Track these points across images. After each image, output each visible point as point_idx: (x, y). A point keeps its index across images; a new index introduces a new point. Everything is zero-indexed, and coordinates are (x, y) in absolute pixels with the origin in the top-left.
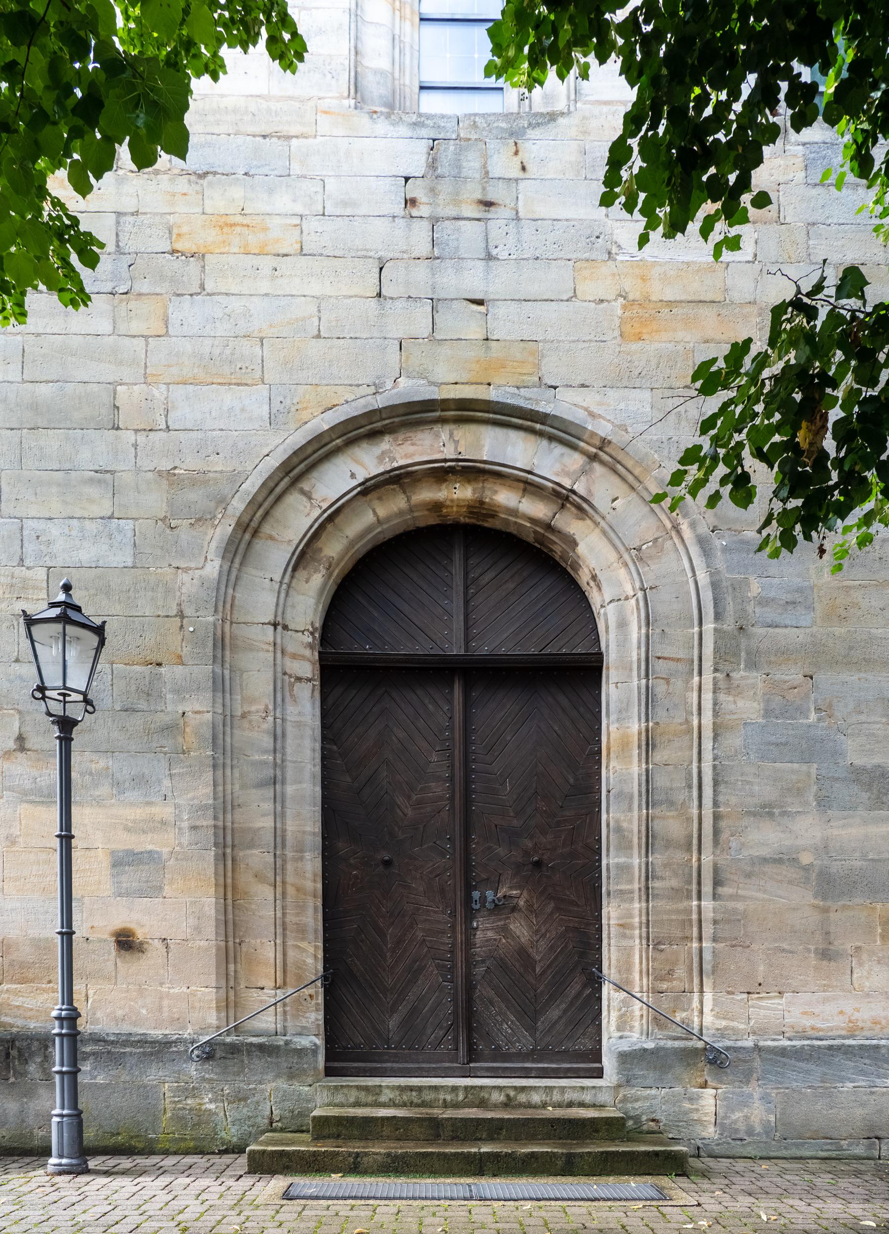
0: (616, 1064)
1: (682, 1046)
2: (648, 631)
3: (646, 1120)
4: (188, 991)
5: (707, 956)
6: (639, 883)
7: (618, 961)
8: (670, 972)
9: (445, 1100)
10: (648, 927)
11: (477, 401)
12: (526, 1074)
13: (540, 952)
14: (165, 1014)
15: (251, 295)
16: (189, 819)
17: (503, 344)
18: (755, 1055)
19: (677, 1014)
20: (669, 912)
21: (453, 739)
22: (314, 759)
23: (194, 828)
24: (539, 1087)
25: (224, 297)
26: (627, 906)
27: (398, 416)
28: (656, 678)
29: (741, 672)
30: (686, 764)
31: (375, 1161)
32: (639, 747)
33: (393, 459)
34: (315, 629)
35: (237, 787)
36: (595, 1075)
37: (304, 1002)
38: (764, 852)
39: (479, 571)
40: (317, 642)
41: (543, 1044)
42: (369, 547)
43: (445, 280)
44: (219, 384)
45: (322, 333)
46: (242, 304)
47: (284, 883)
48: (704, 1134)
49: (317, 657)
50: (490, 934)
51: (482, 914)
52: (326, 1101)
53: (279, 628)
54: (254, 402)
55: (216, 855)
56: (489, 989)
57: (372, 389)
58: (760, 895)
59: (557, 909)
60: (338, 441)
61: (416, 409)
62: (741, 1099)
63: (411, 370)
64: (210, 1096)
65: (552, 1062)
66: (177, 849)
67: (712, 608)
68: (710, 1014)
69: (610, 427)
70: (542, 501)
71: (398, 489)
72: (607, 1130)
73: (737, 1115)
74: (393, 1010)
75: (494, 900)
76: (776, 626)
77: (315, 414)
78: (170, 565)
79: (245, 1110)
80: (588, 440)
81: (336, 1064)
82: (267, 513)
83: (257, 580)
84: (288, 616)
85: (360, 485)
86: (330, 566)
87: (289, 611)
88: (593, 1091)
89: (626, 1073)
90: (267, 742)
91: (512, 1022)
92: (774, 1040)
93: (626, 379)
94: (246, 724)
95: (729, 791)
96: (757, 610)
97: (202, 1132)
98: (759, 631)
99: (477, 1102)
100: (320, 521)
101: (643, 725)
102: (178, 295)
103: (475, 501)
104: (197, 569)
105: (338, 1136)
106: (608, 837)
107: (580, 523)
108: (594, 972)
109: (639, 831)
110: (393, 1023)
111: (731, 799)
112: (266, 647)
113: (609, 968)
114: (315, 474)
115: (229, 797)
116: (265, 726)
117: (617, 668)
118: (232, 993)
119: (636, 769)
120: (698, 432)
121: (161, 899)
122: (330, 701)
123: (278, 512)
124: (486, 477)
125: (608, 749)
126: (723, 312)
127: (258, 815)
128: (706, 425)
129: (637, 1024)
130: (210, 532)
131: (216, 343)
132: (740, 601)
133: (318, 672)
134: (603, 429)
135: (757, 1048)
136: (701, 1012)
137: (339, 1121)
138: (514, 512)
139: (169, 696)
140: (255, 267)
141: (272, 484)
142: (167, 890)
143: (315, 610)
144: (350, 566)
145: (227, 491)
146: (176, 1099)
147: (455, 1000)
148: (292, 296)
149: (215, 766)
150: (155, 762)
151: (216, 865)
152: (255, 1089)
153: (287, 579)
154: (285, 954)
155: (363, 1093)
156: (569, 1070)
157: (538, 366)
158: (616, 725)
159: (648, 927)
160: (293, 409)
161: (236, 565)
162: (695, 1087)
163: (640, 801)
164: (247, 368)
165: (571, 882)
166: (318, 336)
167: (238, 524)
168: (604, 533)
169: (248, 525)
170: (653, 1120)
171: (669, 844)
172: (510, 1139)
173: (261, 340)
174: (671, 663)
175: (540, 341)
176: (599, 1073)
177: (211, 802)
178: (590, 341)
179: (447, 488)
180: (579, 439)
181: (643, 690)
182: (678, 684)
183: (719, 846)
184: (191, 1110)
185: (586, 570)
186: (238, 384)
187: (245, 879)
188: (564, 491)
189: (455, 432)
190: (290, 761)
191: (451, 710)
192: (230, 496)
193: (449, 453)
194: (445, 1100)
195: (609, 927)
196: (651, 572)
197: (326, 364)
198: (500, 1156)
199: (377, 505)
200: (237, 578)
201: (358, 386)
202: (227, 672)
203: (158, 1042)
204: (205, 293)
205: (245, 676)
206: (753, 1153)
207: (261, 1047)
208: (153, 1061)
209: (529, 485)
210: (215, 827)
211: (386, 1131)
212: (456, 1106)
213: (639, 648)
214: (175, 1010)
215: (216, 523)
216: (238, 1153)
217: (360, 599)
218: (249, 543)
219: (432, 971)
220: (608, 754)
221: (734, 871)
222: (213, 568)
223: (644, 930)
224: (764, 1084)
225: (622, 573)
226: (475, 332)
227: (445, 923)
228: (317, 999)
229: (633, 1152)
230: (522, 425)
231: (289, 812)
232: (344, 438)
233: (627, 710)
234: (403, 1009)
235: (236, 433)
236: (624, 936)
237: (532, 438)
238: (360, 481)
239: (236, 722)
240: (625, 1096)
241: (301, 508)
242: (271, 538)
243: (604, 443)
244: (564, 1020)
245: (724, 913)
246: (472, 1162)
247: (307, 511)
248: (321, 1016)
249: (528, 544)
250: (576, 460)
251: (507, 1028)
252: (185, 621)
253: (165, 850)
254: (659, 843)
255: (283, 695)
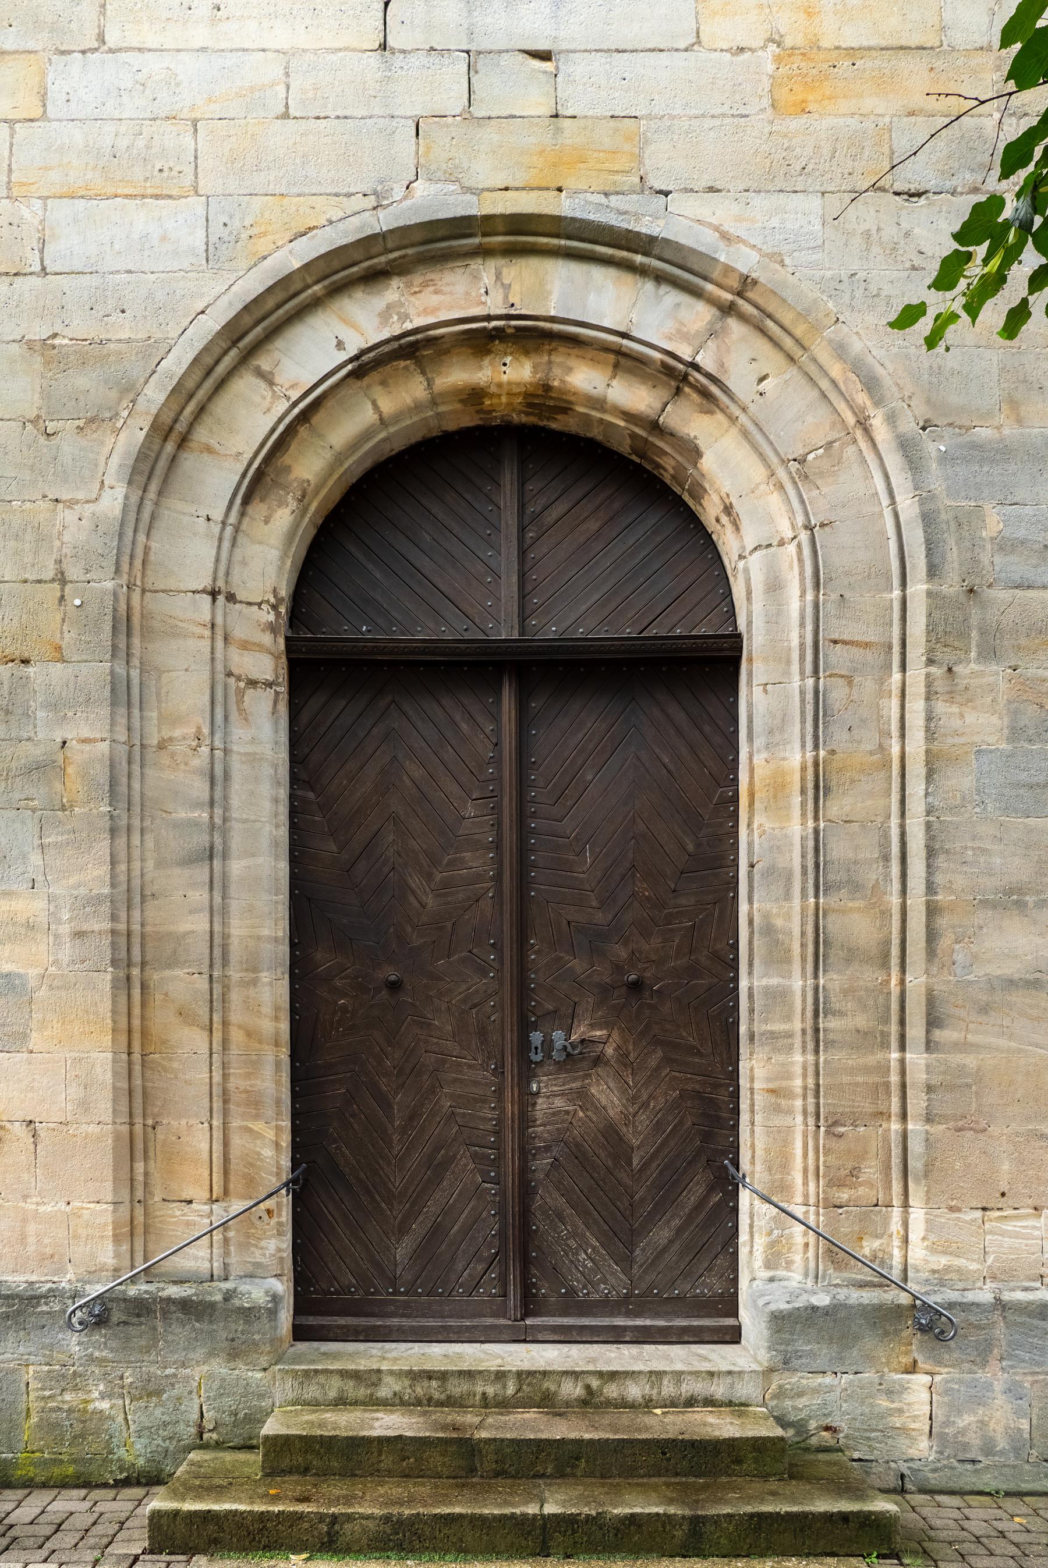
0: (766, 1333)
1: (876, 1301)
2: (817, 596)
3: (816, 1428)
4: (68, 1209)
5: (916, 1146)
6: (803, 1021)
7: (767, 1151)
8: (855, 1172)
9: (484, 1394)
10: (817, 1096)
11: (539, 217)
12: (616, 1337)
13: (640, 1133)
14: (31, 1249)
15: (179, 51)
16: (70, 920)
17: (581, 123)
18: (996, 1316)
19: (865, 1243)
20: (852, 1071)
21: (500, 779)
22: (276, 815)
23: (79, 934)
24: (640, 1372)
25: (137, 54)
26: (781, 1058)
27: (413, 245)
28: (830, 676)
29: (972, 665)
30: (880, 819)
31: (364, 1530)
32: (803, 791)
33: (405, 317)
34: (280, 600)
35: (150, 864)
36: (728, 1338)
37: (258, 1223)
38: (1010, 969)
39: (542, 501)
40: (284, 621)
41: (644, 1286)
42: (368, 464)
43: (489, 20)
44: (126, 196)
45: (291, 111)
46: (165, 65)
47: (225, 1023)
48: (913, 1453)
49: (282, 645)
50: (559, 1103)
51: (545, 1069)
52: (291, 1396)
53: (221, 599)
54: (182, 225)
55: (115, 981)
56: (556, 1194)
57: (371, 201)
58: (1003, 1042)
59: (667, 1060)
60: (316, 288)
61: (441, 233)
62: (973, 1392)
63: (433, 167)
64: (101, 1387)
65: (657, 1315)
66: (52, 970)
67: (923, 556)
68: (922, 1245)
69: (755, 256)
70: (644, 383)
71: (413, 367)
72: (756, 1460)
73: (966, 1420)
74: (403, 1229)
75: (565, 1047)
76: (1029, 587)
77: (280, 244)
78: (45, 497)
79: (158, 1412)
80: (720, 280)
81: (312, 1321)
82: (202, 410)
83: (186, 519)
84: (236, 578)
85: (351, 360)
86: (304, 496)
87: (236, 571)
88: (729, 1380)
89: (783, 1347)
90: (200, 788)
91: (594, 1248)
92: (1026, 1289)
93: (780, 177)
94: (165, 760)
95: (952, 865)
96: (997, 560)
97: (91, 1447)
98: (1001, 595)
99: (537, 1399)
100: (287, 421)
101: (810, 755)
102: (63, 53)
103: (536, 385)
104: (88, 502)
105: (306, 1471)
106: (751, 942)
107: (706, 419)
108: (726, 1167)
109: (803, 934)
110: (402, 1250)
111: (954, 879)
112: (199, 630)
113: (753, 1162)
114: (279, 343)
115: (136, 883)
116: (196, 762)
117: (766, 659)
118: (139, 1211)
119: (796, 828)
120: (997, 171)
121: (25, 1055)
122: (305, 717)
123: (220, 406)
124: (554, 344)
125: (752, 795)
126: (939, 64)
127: (183, 911)
128: (1014, 156)
129: (798, 1258)
130: (110, 440)
131: (123, 129)
132: (968, 544)
133: (286, 671)
134: (744, 260)
135: (1000, 1305)
136: (906, 1241)
137: (309, 1445)
138: (599, 403)
139: (41, 714)
140: (185, 5)
141: (209, 360)
142: (35, 1040)
143: (280, 568)
144: (337, 497)
145: (138, 372)
146: (47, 1393)
147: (502, 1212)
148: (244, 50)
149: (113, 832)
150: (18, 825)
151: (114, 996)
152: (175, 1375)
153: (233, 519)
154: (226, 1144)
155: (351, 1383)
156: (685, 1330)
157: (640, 159)
158: (764, 755)
159: (817, 1096)
160: (244, 236)
161: (152, 495)
162: (896, 1371)
163: (804, 882)
164: (171, 169)
165: (689, 1017)
166: (286, 116)
167: (154, 426)
168: (745, 434)
169: (171, 429)
170: (827, 1428)
171: (852, 955)
172: (592, 1475)
173: (195, 123)
174: (854, 650)
175: (642, 118)
176: (733, 1336)
177: (106, 891)
178: (724, 115)
179: (491, 364)
180: (705, 278)
181: (810, 697)
182: (867, 685)
183: (936, 960)
184: (70, 1411)
185: (715, 498)
186: (157, 197)
187: (162, 1018)
188: (681, 366)
189: (505, 271)
190: (238, 820)
191: (498, 731)
192: (142, 380)
193: (495, 305)
194: (484, 1394)
195: (752, 1093)
196: (821, 502)
197: (297, 161)
198: (577, 1522)
199: (378, 392)
200: (153, 517)
201: (349, 195)
202: (135, 674)
203: (18, 1296)
204: (106, 48)
205: (165, 678)
206: (992, 1485)
207: (185, 1305)
208: (10, 1328)
209: (623, 356)
210: (113, 932)
211: (387, 1461)
212: (504, 1404)
213: (802, 625)
214: (46, 1241)
215: (119, 425)
216: (147, 1485)
217: (353, 549)
218: (174, 459)
219: (466, 1165)
220: (751, 804)
221: (960, 1002)
222: (113, 501)
223: (811, 1100)
224: (1012, 1367)
225: (775, 499)
226: (537, 104)
227: (486, 1084)
228: (280, 1215)
229: (805, 1515)
230: (612, 256)
231: (234, 905)
232: (326, 282)
233: (782, 729)
234: (418, 1228)
235: (153, 277)
236: (777, 1109)
237: (628, 278)
238: (352, 354)
239: (150, 756)
240: (780, 1387)
241: (257, 399)
242: (209, 450)
243: (746, 284)
244: (676, 1247)
245: (944, 1073)
246: (529, 1533)
247: (266, 404)
248: (286, 1243)
249: (621, 457)
250: (698, 315)
251: (584, 1258)
252: (68, 588)
253: (33, 972)
254: (836, 955)
255: (226, 711)
